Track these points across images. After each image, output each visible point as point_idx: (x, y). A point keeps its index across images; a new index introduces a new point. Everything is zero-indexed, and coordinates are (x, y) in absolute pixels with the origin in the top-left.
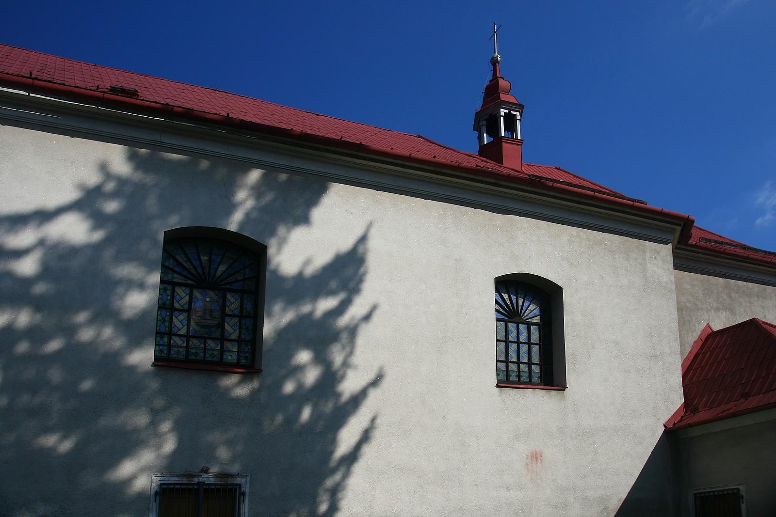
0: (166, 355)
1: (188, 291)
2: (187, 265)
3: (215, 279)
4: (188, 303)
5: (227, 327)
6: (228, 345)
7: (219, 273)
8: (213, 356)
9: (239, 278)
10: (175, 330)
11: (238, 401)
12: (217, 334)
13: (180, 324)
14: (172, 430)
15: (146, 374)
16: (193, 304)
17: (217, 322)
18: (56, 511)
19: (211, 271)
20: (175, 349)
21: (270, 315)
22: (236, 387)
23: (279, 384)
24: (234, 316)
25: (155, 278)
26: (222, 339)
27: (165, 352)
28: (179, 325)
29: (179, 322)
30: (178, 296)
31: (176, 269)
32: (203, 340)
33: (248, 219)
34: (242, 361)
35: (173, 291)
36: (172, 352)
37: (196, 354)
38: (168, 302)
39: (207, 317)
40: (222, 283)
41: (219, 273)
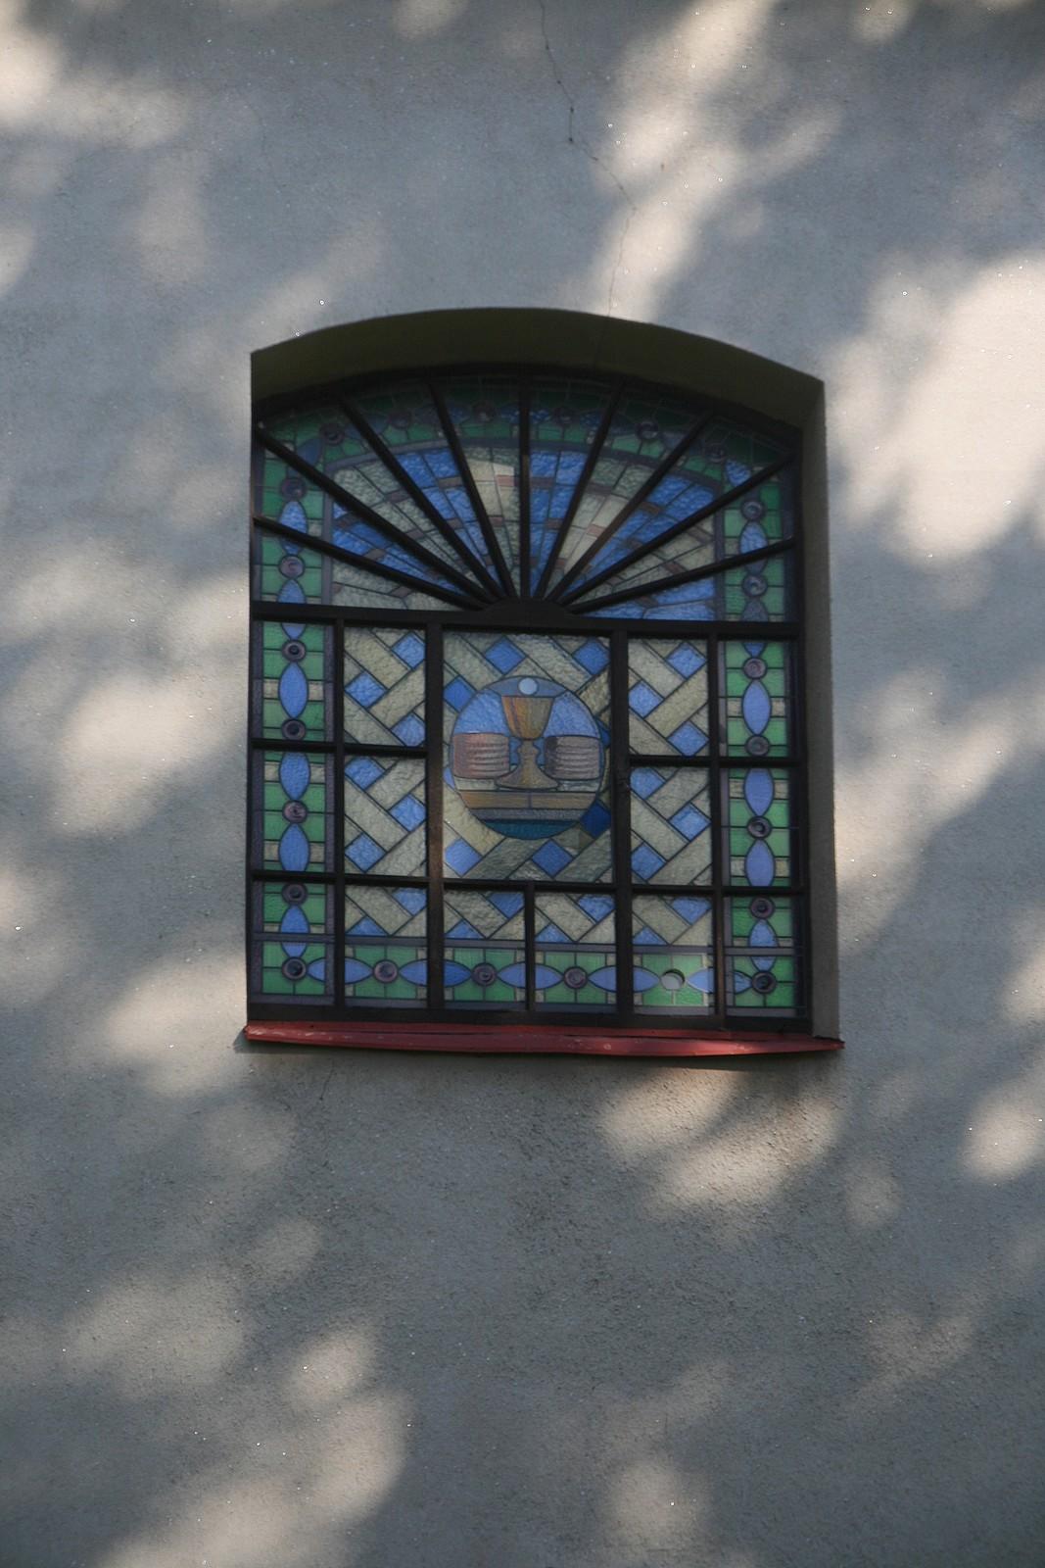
0: (319, 989)
1: (414, 648)
2: (404, 517)
3: (556, 579)
4: (421, 712)
5: (641, 819)
6: (653, 917)
7: (576, 547)
8: (576, 979)
9: (693, 562)
10: (359, 857)
11: (699, 1224)
12: (596, 861)
13: (389, 823)
14: (372, 1385)
15: (205, 1105)
16: (448, 716)
17: (586, 802)
18: (544, 1309)
19: (535, 537)
20: (371, 954)
21: (866, 748)
22: (698, 1143)
23: (947, 1122)
24: (680, 762)
25: (222, 611)
26: (623, 888)
27: (318, 971)
28: (384, 830)
29: (380, 811)
30: (366, 682)
31: (340, 540)
32: (516, 900)
33: (712, 239)
34: (742, 1001)
35: (337, 656)
36: (352, 971)
37: (484, 975)
38: (313, 717)
39: (535, 778)
40: (603, 591)
41: (576, 547)
